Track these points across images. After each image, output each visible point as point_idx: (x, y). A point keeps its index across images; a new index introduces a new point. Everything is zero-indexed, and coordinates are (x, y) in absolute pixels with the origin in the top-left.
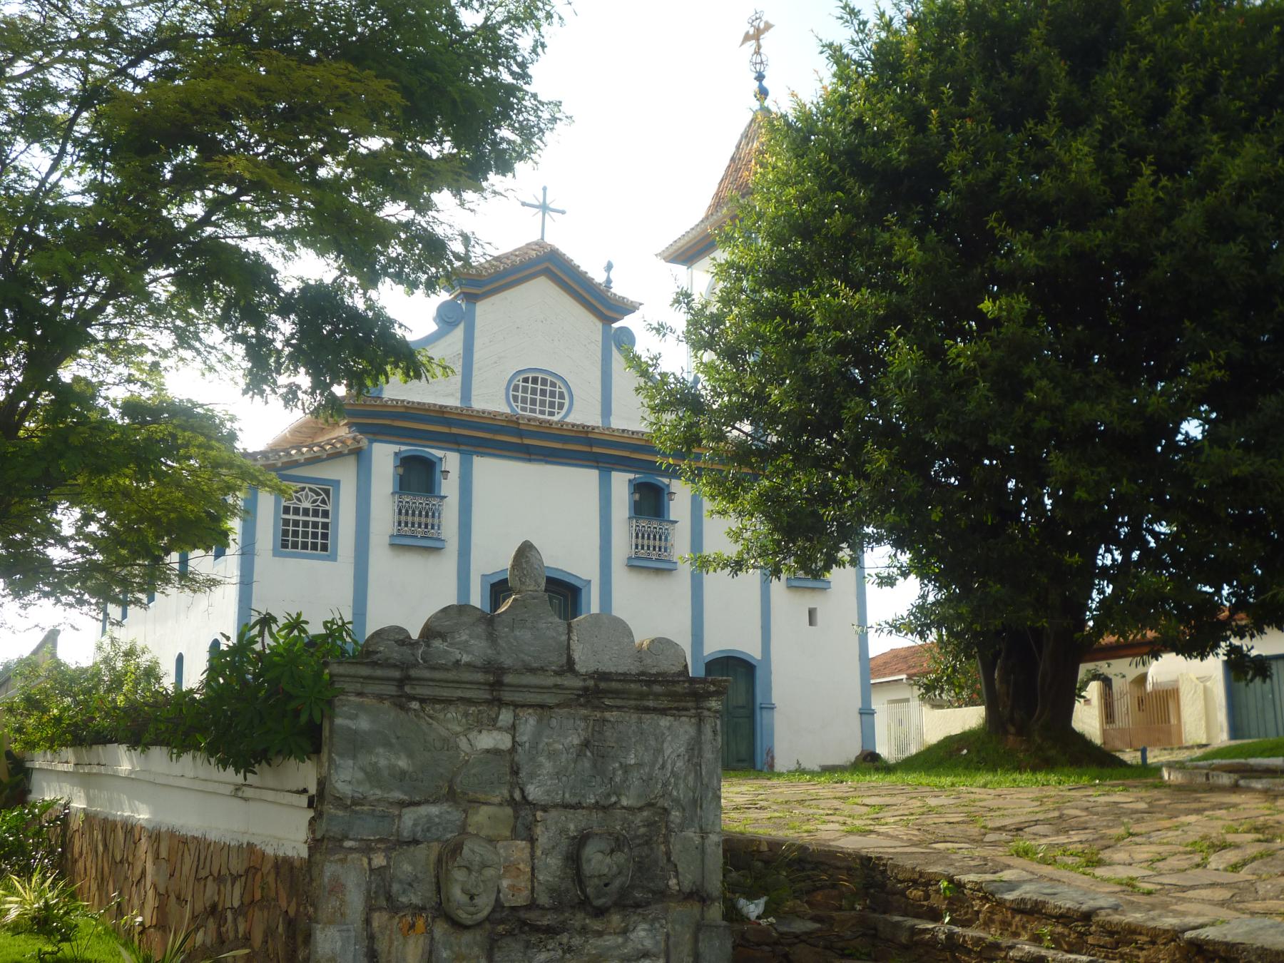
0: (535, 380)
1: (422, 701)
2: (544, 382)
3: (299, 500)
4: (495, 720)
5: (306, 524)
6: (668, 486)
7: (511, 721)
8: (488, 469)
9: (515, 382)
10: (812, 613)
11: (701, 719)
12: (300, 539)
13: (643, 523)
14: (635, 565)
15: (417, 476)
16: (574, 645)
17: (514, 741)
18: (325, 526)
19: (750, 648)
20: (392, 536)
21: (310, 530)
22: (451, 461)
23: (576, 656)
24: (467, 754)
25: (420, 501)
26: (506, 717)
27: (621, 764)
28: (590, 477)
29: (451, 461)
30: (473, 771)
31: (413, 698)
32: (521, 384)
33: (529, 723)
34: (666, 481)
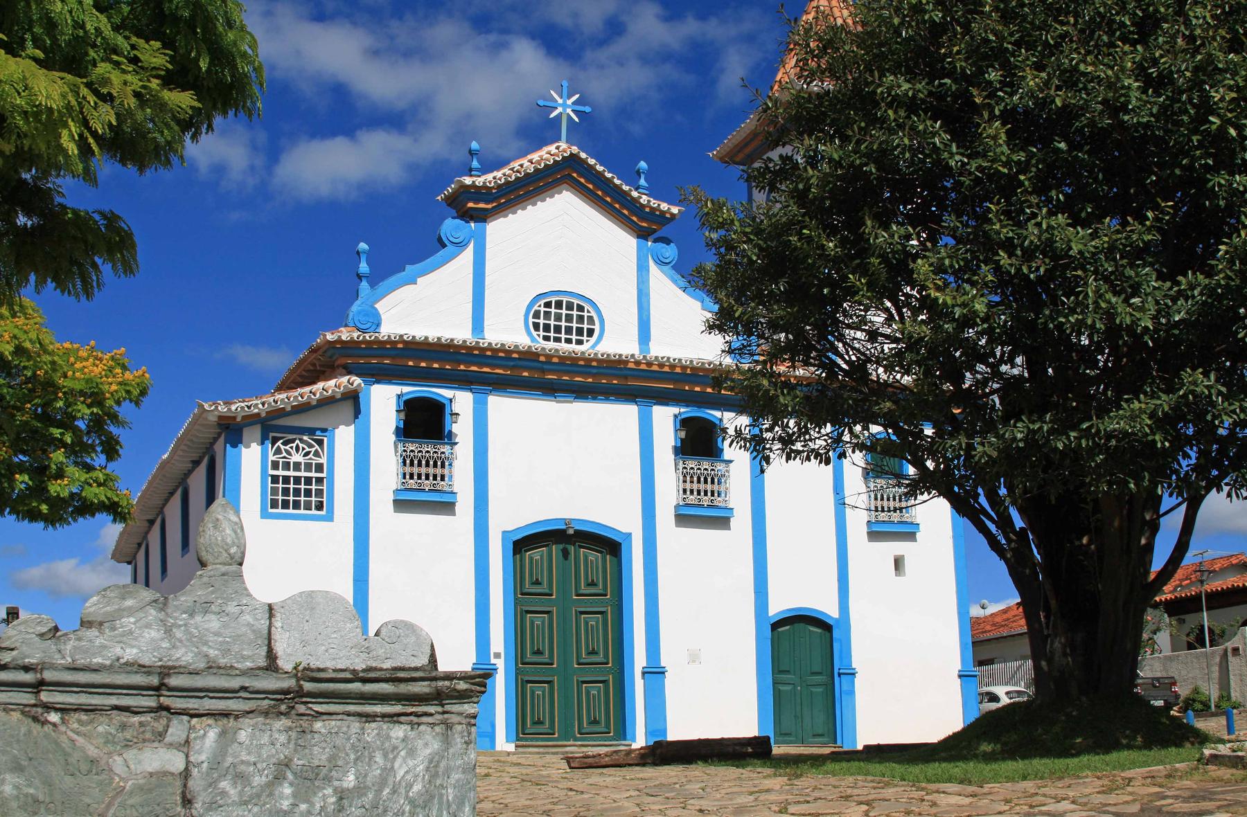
0: (559, 305)
1: (64, 710)
2: (570, 306)
3: (289, 454)
4: (161, 736)
5: (297, 480)
6: (721, 420)
7: (184, 736)
8: (501, 406)
9: (536, 308)
10: (898, 563)
11: (449, 726)
12: (313, 499)
13: (691, 464)
14: (683, 519)
15: (424, 422)
16: (277, 635)
17: (188, 762)
18: (320, 481)
19: (828, 608)
20: (396, 491)
21: (303, 487)
22: (461, 402)
23: (279, 648)
24: (121, 779)
25: (428, 448)
26: (177, 729)
27: (335, 790)
28: (628, 413)
29: (461, 402)
30: (130, 802)
31: (48, 707)
32: (543, 309)
33: (209, 736)
34: (718, 414)
